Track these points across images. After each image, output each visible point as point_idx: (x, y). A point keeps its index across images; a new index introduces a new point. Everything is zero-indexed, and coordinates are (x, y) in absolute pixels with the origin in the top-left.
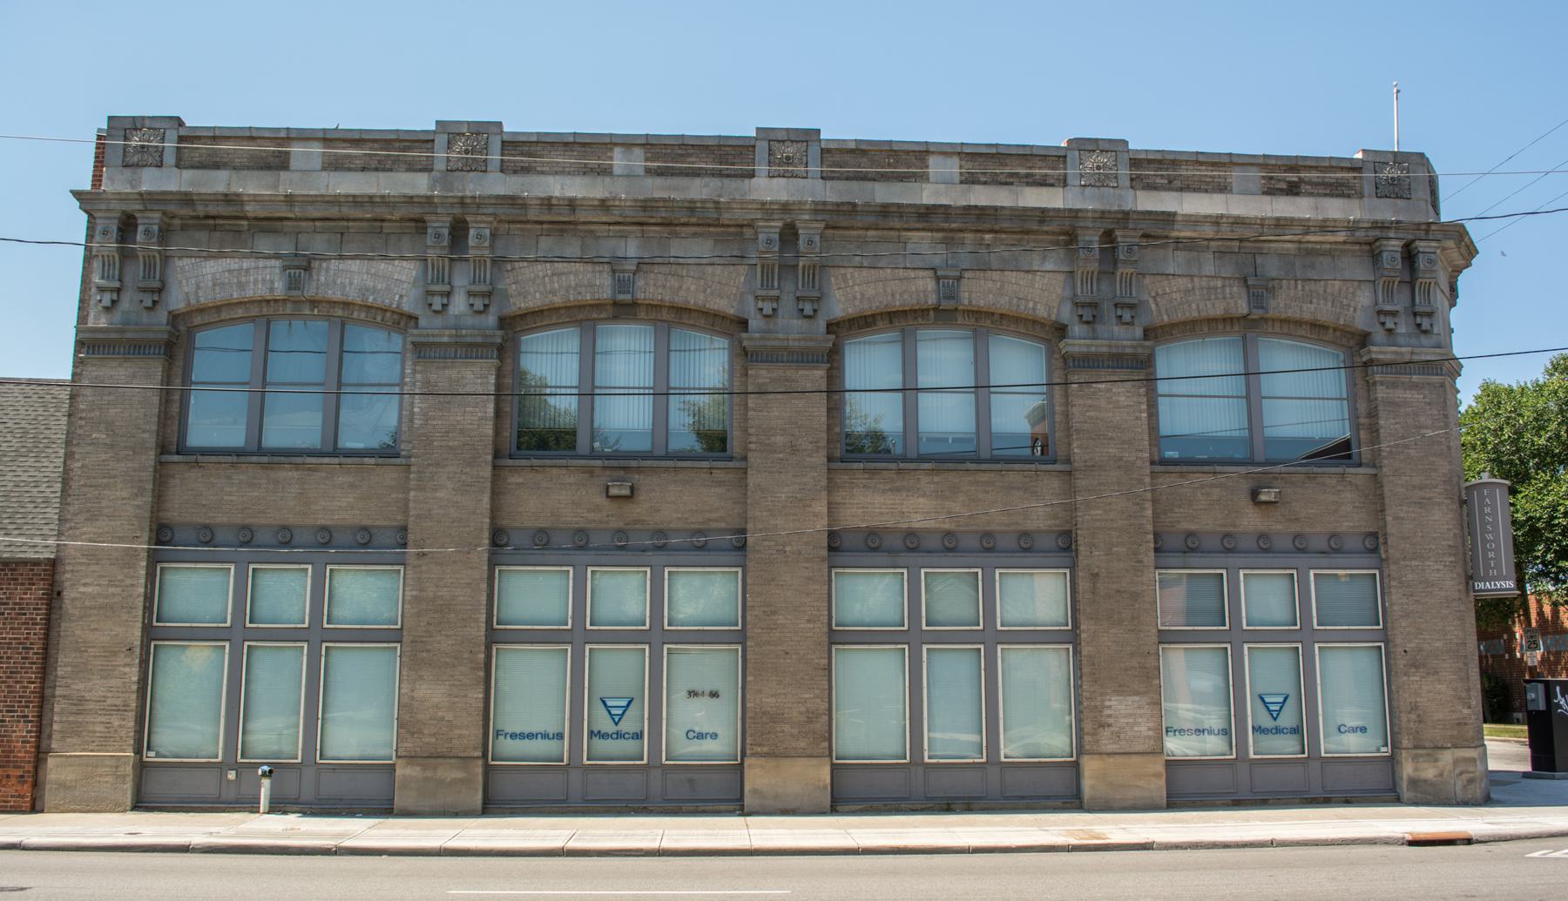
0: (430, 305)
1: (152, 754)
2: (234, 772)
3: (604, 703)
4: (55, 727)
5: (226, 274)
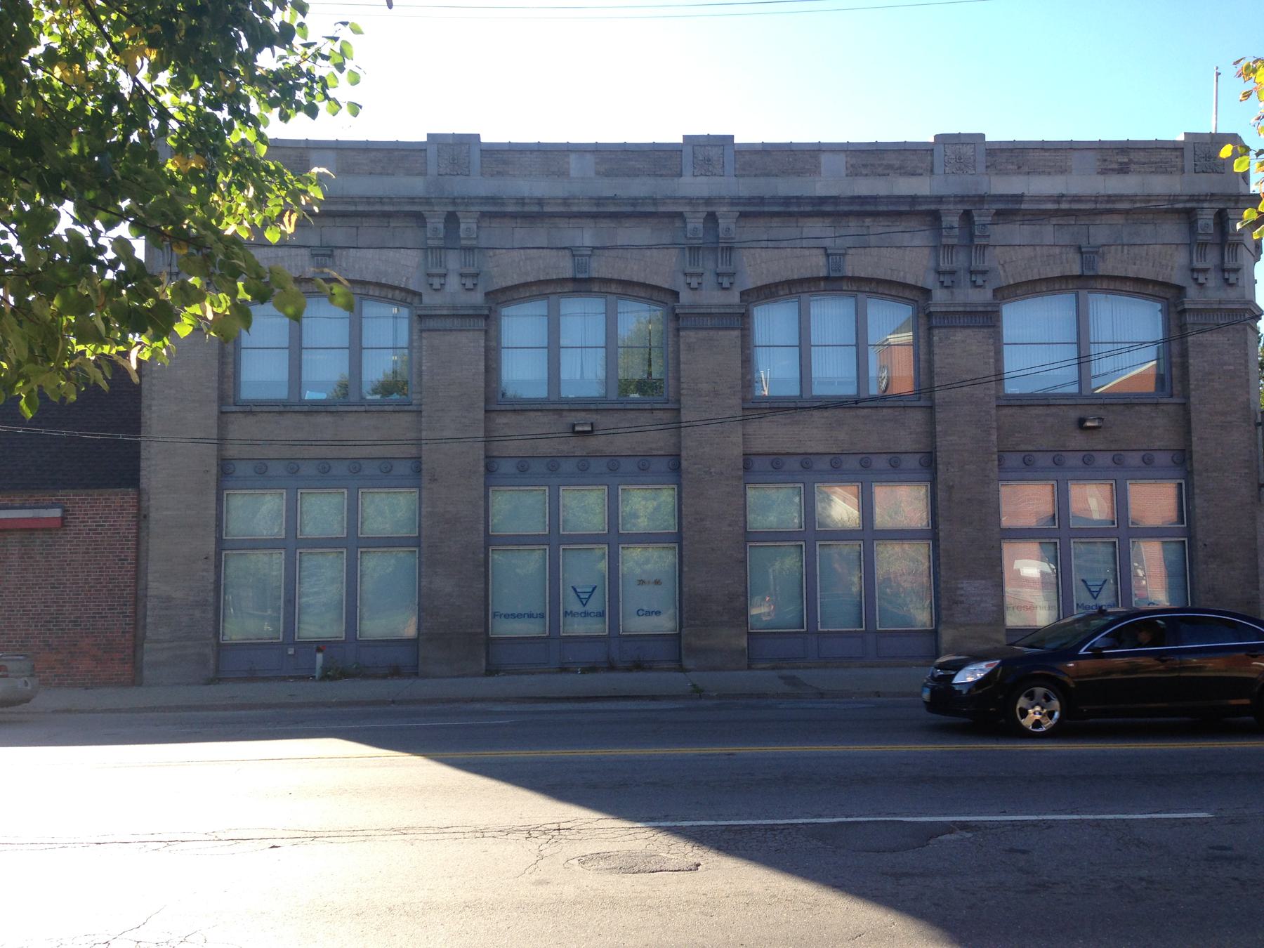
0: (431, 285)
2: (290, 653)
3: (575, 589)
4: (149, 620)
5: (265, 260)
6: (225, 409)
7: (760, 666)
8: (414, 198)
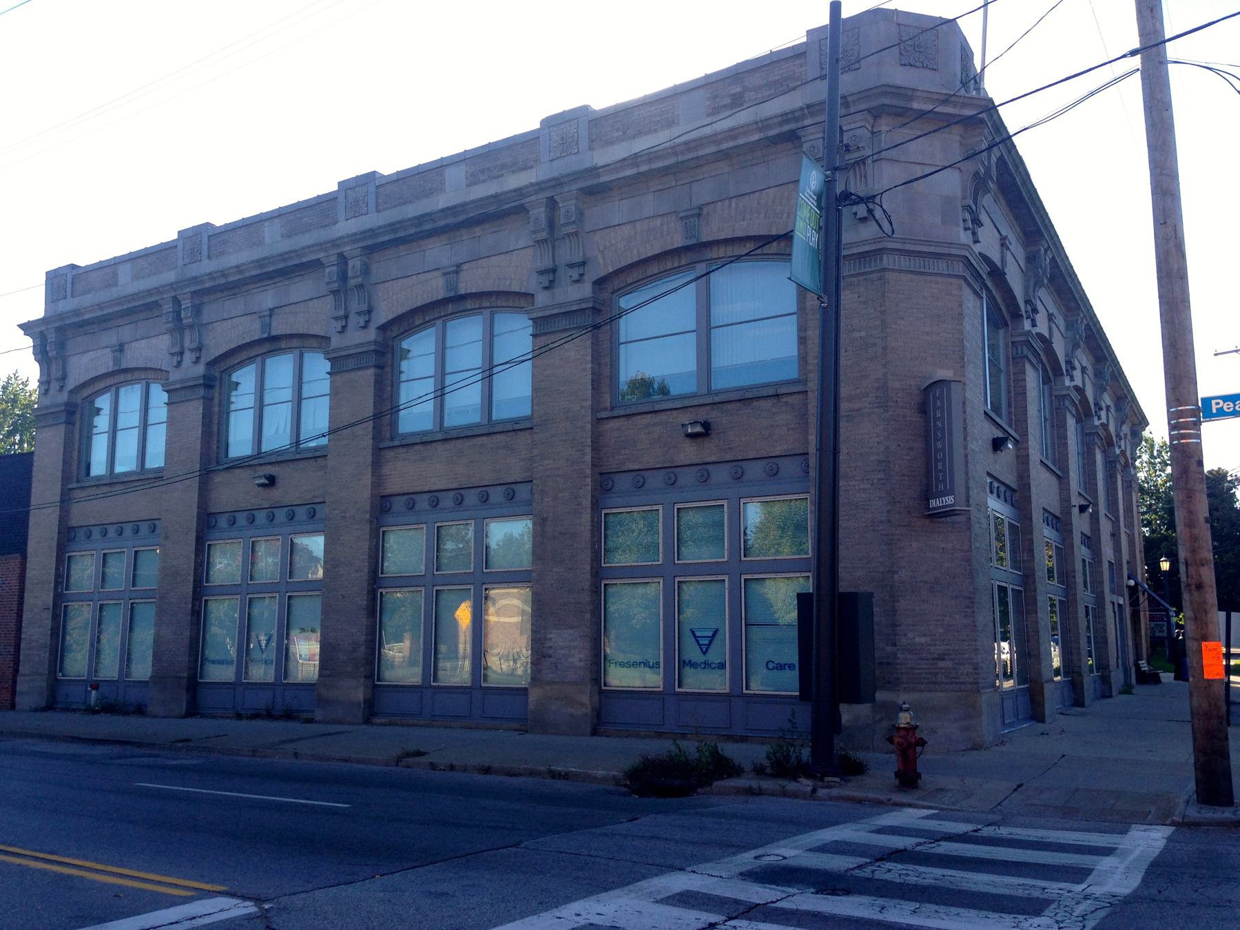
1: (61, 674)
3: (693, 632)
6: (382, 445)
7: (379, 721)
8: (149, 291)
